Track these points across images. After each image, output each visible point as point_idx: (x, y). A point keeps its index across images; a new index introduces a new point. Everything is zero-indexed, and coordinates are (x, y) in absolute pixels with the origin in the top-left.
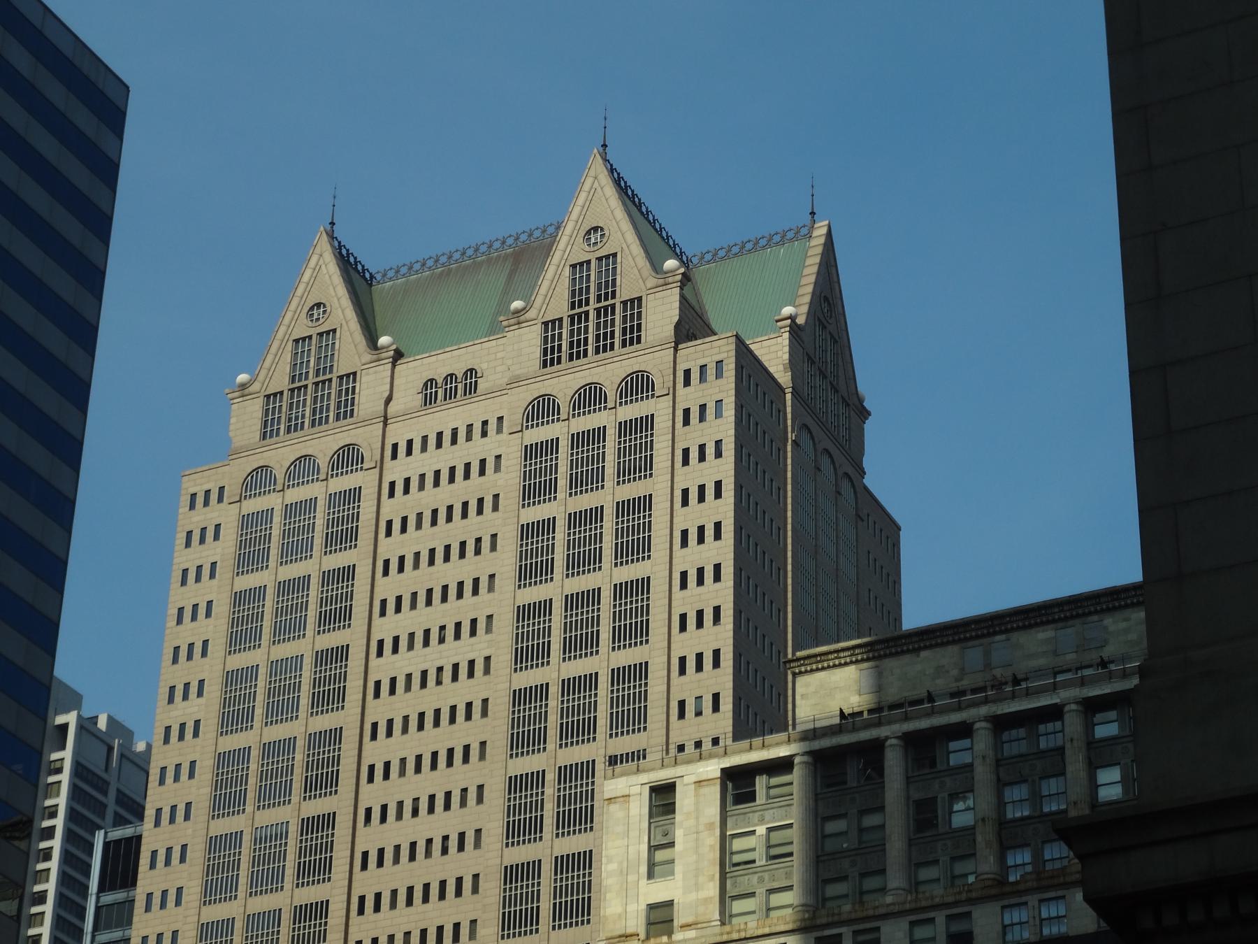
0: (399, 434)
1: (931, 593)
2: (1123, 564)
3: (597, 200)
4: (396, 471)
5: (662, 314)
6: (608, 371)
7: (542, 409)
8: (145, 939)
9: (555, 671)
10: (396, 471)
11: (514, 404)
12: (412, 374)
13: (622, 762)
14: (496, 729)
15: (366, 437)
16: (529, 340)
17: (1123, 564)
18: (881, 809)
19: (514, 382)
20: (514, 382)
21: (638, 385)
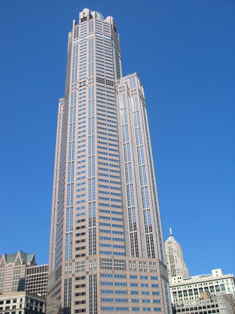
0: (7, 268)
1: (25, 292)
2: (220, 269)
3: (19, 254)
4: (7, 271)
5: (22, 262)
6: (19, 266)
7: (15, 268)
8: (20, 312)
9: (15, 281)
10: (7, 271)
11: (13, 267)
12: (9, 264)
13: (81, 226)
14: (12, 278)
15: (5, 268)
16: (15, 263)
17: (220, 269)
18: (176, 295)
19: (14, 266)
20: (14, 266)
21: (20, 267)
